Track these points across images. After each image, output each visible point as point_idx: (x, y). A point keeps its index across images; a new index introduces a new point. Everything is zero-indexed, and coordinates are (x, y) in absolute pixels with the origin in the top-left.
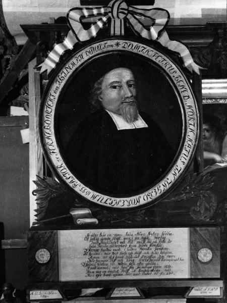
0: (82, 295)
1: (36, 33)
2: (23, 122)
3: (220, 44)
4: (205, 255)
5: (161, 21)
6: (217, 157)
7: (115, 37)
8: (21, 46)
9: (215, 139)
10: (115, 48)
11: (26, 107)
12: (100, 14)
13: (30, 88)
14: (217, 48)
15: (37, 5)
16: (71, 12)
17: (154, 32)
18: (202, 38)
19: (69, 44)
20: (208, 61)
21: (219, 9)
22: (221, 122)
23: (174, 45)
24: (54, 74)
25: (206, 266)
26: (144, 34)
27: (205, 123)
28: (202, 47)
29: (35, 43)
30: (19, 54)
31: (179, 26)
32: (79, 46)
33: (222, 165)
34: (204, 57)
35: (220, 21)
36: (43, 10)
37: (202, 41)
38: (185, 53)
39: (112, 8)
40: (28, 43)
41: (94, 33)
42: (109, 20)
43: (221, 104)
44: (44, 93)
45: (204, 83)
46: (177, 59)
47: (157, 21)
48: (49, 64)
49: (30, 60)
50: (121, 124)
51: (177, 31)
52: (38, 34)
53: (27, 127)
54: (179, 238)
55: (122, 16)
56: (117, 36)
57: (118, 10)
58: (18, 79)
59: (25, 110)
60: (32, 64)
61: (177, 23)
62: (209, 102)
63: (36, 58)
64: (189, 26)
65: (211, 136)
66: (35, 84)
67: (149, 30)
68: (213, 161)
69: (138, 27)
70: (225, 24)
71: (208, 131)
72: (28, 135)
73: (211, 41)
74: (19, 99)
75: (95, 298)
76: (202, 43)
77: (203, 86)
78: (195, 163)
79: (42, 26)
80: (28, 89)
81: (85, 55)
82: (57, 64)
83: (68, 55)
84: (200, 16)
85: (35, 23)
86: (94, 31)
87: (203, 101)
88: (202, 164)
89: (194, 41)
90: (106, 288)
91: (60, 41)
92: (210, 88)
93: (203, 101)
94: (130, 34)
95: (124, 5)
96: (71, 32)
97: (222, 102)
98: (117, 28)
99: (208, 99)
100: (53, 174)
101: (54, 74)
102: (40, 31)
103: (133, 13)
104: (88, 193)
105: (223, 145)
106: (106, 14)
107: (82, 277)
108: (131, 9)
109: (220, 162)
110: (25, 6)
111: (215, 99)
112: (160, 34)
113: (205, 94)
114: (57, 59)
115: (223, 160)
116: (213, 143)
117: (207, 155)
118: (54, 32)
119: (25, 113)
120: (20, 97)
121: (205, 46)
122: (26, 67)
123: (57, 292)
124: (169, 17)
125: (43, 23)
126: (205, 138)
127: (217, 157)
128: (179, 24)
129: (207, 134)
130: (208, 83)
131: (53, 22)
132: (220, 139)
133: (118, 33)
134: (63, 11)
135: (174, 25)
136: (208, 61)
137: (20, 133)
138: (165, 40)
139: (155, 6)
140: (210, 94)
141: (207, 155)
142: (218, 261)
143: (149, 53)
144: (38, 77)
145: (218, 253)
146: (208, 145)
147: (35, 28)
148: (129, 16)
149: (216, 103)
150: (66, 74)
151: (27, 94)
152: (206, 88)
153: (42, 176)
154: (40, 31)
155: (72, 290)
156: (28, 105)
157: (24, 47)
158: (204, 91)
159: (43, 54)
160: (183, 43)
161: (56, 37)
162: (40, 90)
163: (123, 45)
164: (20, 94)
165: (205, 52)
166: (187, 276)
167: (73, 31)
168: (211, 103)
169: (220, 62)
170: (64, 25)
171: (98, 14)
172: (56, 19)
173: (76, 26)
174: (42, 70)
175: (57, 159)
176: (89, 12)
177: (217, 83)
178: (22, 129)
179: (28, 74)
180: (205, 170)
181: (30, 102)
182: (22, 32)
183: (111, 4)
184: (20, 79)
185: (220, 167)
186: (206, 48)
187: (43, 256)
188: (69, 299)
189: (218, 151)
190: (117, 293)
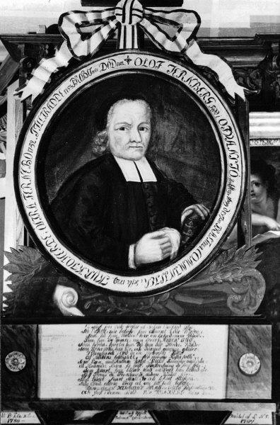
1: (19, 46)
3: (274, 63)
4: (250, 363)
6: (271, 223)
9: (268, 197)
10: (126, 66)
12: (99, 21)
14: (271, 69)
16: (195, 24)
21: (273, 16)
22: (276, 173)
25: (244, 377)
27: (252, 173)
28: (249, 68)
29: (17, 60)
31: (217, 38)
32: (76, 63)
35: (274, 32)
37: (248, 59)
42: (118, 25)
43: (59, 190)
45: (252, 118)
48: (34, 87)
49: (9, 84)
50: (130, 174)
52: (22, 47)
54: (214, 338)
55: (135, 20)
56: (122, 50)
57: (131, 12)
60: (12, 90)
62: (260, 144)
65: (262, 192)
66: (16, 116)
67: (174, 39)
68: (265, 229)
69: (159, 37)
71: (257, 184)
73: (262, 59)
76: (249, 63)
77: (251, 121)
78: (241, 232)
83: (58, 78)
86: (95, 42)
88: (249, 231)
89: (238, 60)
91: (51, 54)
92: (260, 125)
93: (251, 142)
94: (146, 45)
95: (138, 5)
96: (65, 44)
102: (25, 44)
103: (153, 20)
104: (83, 269)
107: (73, 391)
108: (147, 12)
109: (275, 230)
111: (267, 139)
116: (264, 202)
117: (132, 266)
118: (45, 44)
121: (253, 65)
122: (4, 93)
123: (33, 414)
124: (199, 21)
125: (30, 33)
126: (254, 195)
127: (271, 223)
128: (217, 36)
129: (256, 189)
130: (258, 118)
131: (43, 31)
135: (211, 36)
138: (194, 53)
140: (260, 132)
141: (257, 219)
142: (268, 375)
144: (21, 106)
145: (269, 362)
146: (257, 204)
148: (146, 23)
149: (269, 145)
151: (4, 129)
154: (25, 44)
156: (5, 146)
157: (2, 65)
158: (252, 129)
159: (23, 75)
160: (226, 61)
161: (47, 52)
163: (149, 62)
165: (253, 74)
166: (221, 396)
167: (69, 45)
169: (275, 88)
170: (57, 35)
171: (96, 20)
173: (75, 38)
174: (24, 96)
175: (45, 233)
177: (270, 117)
179: (6, 103)
180: (253, 240)
183: (120, 5)
186: (253, 68)
187: (17, 362)
189: (272, 213)
190: (121, 418)
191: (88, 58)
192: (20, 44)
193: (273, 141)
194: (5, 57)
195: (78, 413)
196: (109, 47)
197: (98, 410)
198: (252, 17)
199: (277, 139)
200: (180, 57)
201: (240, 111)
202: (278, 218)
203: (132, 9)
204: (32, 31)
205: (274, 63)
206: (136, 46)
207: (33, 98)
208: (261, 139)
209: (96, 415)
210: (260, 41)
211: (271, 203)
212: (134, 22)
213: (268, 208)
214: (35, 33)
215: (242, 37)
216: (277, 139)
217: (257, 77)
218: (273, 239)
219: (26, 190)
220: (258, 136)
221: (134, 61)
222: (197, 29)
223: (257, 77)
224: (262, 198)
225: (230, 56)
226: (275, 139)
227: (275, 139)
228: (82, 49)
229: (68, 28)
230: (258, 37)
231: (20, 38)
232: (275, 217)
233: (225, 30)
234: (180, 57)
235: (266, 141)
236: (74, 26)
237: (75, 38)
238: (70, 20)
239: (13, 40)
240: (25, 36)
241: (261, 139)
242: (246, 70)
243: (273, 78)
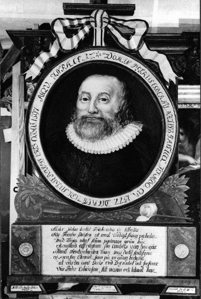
0: (58, 289)
1: (21, 38)
2: (6, 122)
5: (140, 30)
6: (191, 160)
7: (97, 48)
8: (6, 51)
11: (9, 106)
13: (13, 90)
15: (22, 11)
17: (134, 43)
18: (178, 46)
19: (54, 51)
20: (183, 68)
21: (195, 19)
22: (195, 126)
26: (123, 41)
28: (177, 54)
30: (4, 59)
32: (63, 55)
34: (179, 65)
36: (27, 17)
37: (178, 49)
38: (163, 61)
39: (95, 18)
40: (13, 47)
41: (76, 44)
42: (92, 29)
44: (29, 98)
45: (180, 89)
46: (153, 67)
47: (137, 31)
49: (13, 65)
51: (152, 40)
53: (10, 127)
55: (105, 25)
56: (98, 47)
59: (8, 110)
60: (16, 69)
61: (154, 31)
62: (184, 106)
63: (19, 63)
64: (166, 34)
65: (185, 139)
68: (187, 164)
70: (196, 34)
72: (12, 135)
73: (186, 49)
74: (3, 100)
75: (71, 292)
76: (178, 51)
77: (179, 91)
78: (175, 166)
79: (26, 31)
80: (11, 91)
81: (71, 63)
82: (42, 71)
85: (20, 29)
86: (75, 40)
89: (170, 49)
90: (83, 285)
92: (185, 94)
94: (111, 43)
95: (105, 14)
96: (56, 41)
98: (98, 40)
99: (183, 104)
100: (34, 167)
101: (39, 80)
106: (88, 23)
109: (194, 165)
110: (11, 12)
111: (189, 104)
113: (181, 99)
114: (41, 66)
115: (196, 162)
116: (187, 145)
117: (181, 157)
118: (38, 37)
119: (9, 114)
120: (3, 98)
122: (10, 70)
125: (27, 29)
127: (191, 160)
130: (183, 89)
131: (37, 28)
132: (193, 141)
133: (99, 44)
134: (49, 18)
135: (152, 32)
136: (183, 68)
137: (3, 133)
140: (185, 99)
141: (181, 157)
143: (131, 64)
146: (182, 147)
148: (110, 27)
150: (50, 80)
152: (181, 94)
153: (23, 173)
155: (52, 286)
157: (9, 51)
158: (179, 97)
159: (27, 61)
162: (23, 92)
164: (4, 96)
166: (163, 274)
172: (40, 25)
173: (62, 36)
175: (40, 157)
176: (70, 22)
177: (192, 89)
178: (5, 128)
181: (13, 103)
184: (4, 81)
185: (193, 169)
186: (182, 55)
188: (48, 293)
189: (191, 153)
191: (73, 52)
192: (21, 36)
193: (193, 105)
195: (60, 284)
196: (86, 44)
197: (73, 282)
198: (180, 20)
199: (196, 104)
200: (134, 54)
201: (172, 91)
202: (195, 157)
203: (101, 18)
204: (29, 27)
205: (195, 52)
206: (103, 45)
207: (33, 78)
208: (185, 104)
209: (73, 287)
210: (185, 37)
211: (191, 147)
212: (104, 26)
213: (189, 150)
214: (32, 29)
215: (170, 34)
216: (196, 104)
217: (183, 61)
219: (34, 139)
220: (183, 101)
221: (102, 55)
222: (146, 33)
223: (183, 61)
224: (185, 144)
226: (194, 104)
227: (194, 104)
228: (68, 44)
229: (58, 28)
230: (184, 33)
231: (20, 32)
232: (194, 156)
233: (161, 28)
234: (134, 54)
235: (188, 105)
236: (62, 28)
237: (62, 36)
238: (62, 23)
239: (16, 34)
240: (24, 31)
241: (185, 104)
242: (176, 56)
243: (194, 61)
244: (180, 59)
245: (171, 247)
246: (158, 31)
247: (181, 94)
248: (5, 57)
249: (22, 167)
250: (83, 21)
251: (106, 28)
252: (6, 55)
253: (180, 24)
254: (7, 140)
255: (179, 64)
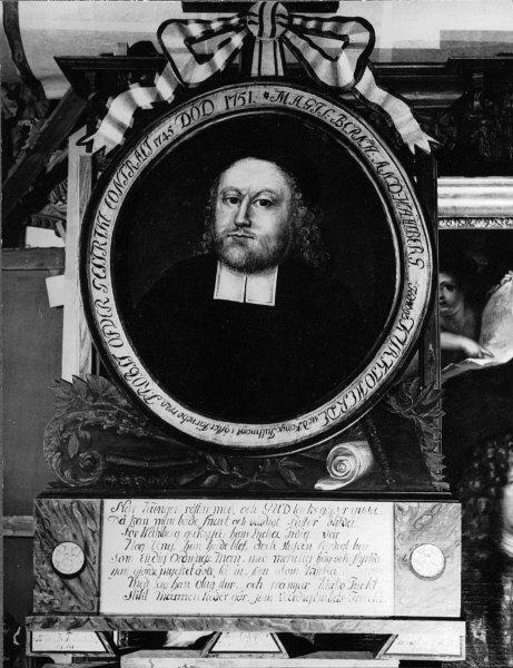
8: (55, 102)
9: (465, 307)
20: (451, 140)
23: (378, 95)
24: (118, 155)
26: (323, 72)
33: (482, 363)
48: (108, 135)
51: (399, 76)
55: (280, 30)
58: (45, 168)
59: (58, 234)
62: (454, 225)
65: (457, 299)
68: (461, 355)
71: (450, 287)
73: (458, 96)
74: (46, 211)
77: (440, 191)
80: (66, 192)
83: (144, 121)
84: (437, 46)
85: (87, 54)
87: (441, 223)
88: (438, 359)
92: (455, 197)
97: (480, 225)
105: (484, 319)
109: (476, 357)
111: (465, 219)
112: (358, 75)
127: (470, 346)
130: (451, 185)
131: (124, 52)
134: (148, 30)
137: (45, 285)
139: (340, 12)
140: (454, 208)
141: (448, 340)
147: (84, 65)
149: (469, 227)
152: (446, 196)
157: (60, 104)
158: (441, 203)
160: (409, 103)
164: (48, 202)
168: (457, 228)
182: (60, 72)
184: (49, 169)
194: (66, 91)
198: (443, 33)
202: (481, 339)
204: (108, 51)
207: (107, 151)
213: (467, 323)
214: (111, 55)
216: (481, 219)
217: (451, 123)
218: (473, 371)
223: (451, 123)
225: (409, 92)
227: (477, 219)
230: (451, 63)
232: (477, 336)
233: (400, 51)
235: (463, 222)
244: (443, 119)
245: (91, 561)
246: (394, 58)
247: (446, 196)
248: (52, 115)
249: (86, 364)
250: (216, 26)
251: (283, 39)
252: (55, 112)
253: (442, 42)
254: (53, 303)
255: (442, 132)
